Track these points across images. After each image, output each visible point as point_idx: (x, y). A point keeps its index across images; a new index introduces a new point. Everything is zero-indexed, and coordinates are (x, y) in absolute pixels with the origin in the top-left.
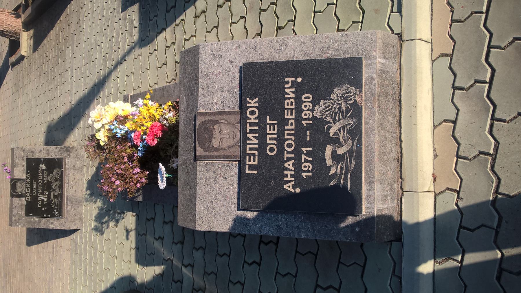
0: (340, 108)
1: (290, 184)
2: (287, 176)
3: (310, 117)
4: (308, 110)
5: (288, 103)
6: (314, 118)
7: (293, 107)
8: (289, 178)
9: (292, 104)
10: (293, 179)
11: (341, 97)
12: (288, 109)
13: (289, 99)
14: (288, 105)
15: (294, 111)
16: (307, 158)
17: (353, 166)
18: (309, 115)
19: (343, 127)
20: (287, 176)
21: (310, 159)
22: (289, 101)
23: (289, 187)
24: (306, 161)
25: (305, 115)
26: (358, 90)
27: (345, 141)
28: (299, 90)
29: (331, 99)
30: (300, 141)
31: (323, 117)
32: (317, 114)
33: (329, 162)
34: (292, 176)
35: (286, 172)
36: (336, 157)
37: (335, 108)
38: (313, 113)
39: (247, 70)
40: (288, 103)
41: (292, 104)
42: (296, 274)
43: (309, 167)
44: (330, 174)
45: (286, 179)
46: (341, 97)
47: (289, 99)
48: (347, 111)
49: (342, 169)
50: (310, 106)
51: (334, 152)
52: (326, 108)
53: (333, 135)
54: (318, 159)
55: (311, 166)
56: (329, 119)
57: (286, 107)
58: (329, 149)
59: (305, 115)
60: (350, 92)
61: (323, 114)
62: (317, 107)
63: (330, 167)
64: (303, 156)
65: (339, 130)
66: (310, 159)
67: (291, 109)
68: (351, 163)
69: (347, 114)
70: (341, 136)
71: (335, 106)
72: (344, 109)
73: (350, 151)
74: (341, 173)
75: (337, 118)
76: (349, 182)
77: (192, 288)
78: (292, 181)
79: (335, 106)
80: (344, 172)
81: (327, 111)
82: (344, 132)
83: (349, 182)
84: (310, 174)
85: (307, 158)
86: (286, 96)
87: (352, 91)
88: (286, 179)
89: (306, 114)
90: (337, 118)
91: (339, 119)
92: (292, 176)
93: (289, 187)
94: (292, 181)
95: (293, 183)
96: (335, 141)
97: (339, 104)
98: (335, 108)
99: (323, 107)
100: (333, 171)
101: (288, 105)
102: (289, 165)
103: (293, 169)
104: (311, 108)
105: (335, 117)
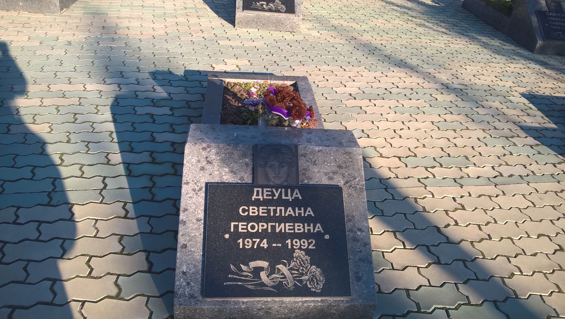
0: (302, 274)
1: (292, 213)
2: (300, 209)
3: (294, 247)
4: (301, 245)
5: (300, 226)
6: (293, 250)
7: (296, 231)
8: (297, 211)
9: (298, 230)
10: (297, 215)
11: (313, 275)
12: (294, 225)
13: (304, 227)
14: (298, 226)
15: (293, 231)
16: (256, 243)
17: (250, 287)
18: (296, 246)
19: (285, 277)
20: (300, 209)
21: (255, 247)
22: (301, 228)
23: (290, 212)
24: (254, 243)
25: (296, 242)
26: (320, 291)
27: (273, 279)
28: (317, 236)
29: (311, 266)
30: (272, 236)
31: (295, 259)
32: (297, 253)
33: (253, 264)
34: (300, 214)
35: (302, 208)
36: (258, 270)
37: (302, 270)
38: (298, 249)
39: (207, 184)
40: (300, 226)
41: (298, 230)
42: (154, 233)
43: (248, 246)
44: (241, 265)
45: (297, 209)
46: (313, 275)
47: (304, 227)
48: (301, 281)
49: (247, 276)
50: (304, 246)
51: (262, 269)
52: (303, 261)
53: (278, 269)
54: (258, 253)
55: (248, 247)
56: (293, 264)
57: (296, 224)
58: (265, 264)
59: (296, 242)
60: (318, 284)
61: (297, 258)
62: (304, 253)
63: (248, 265)
64: (258, 240)
65: (283, 274)
66: (255, 247)
67: (294, 229)
68: (251, 285)
69: (298, 281)
70: (277, 276)
71: (304, 269)
72: (302, 278)
73: (263, 284)
74: (243, 276)
75: (294, 272)
76: (231, 283)
77: (16, 304)
78: (295, 214)
79: (304, 269)
80: (243, 278)
81: (300, 263)
82: (281, 278)
83: (231, 283)
84: (241, 247)
85: (256, 243)
86: (283, 231)
87: (319, 286)
88: (297, 209)
89: (297, 243)
90: (294, 272)
91: (292, 274)
92: (300, 214)
93: (290, 212)
94: (295, 214)
95: (294, 215)
96: (272, 270)
97: (306, 273)
98: (302, 270)
99: (304, 259)
100: (244, 267)
101: (298, 226)
102: (309, 212)
103: (315, 231)
104: (302, 247)
105: (294, 270)
